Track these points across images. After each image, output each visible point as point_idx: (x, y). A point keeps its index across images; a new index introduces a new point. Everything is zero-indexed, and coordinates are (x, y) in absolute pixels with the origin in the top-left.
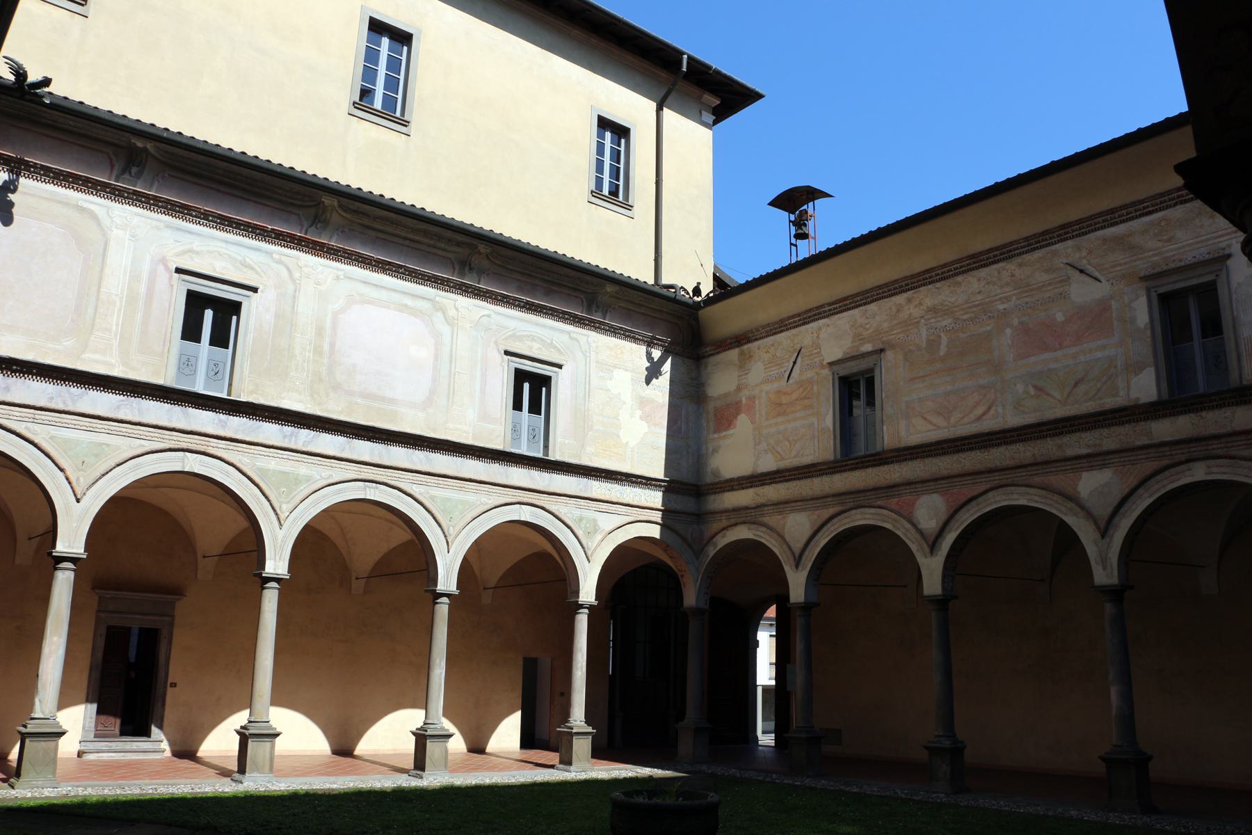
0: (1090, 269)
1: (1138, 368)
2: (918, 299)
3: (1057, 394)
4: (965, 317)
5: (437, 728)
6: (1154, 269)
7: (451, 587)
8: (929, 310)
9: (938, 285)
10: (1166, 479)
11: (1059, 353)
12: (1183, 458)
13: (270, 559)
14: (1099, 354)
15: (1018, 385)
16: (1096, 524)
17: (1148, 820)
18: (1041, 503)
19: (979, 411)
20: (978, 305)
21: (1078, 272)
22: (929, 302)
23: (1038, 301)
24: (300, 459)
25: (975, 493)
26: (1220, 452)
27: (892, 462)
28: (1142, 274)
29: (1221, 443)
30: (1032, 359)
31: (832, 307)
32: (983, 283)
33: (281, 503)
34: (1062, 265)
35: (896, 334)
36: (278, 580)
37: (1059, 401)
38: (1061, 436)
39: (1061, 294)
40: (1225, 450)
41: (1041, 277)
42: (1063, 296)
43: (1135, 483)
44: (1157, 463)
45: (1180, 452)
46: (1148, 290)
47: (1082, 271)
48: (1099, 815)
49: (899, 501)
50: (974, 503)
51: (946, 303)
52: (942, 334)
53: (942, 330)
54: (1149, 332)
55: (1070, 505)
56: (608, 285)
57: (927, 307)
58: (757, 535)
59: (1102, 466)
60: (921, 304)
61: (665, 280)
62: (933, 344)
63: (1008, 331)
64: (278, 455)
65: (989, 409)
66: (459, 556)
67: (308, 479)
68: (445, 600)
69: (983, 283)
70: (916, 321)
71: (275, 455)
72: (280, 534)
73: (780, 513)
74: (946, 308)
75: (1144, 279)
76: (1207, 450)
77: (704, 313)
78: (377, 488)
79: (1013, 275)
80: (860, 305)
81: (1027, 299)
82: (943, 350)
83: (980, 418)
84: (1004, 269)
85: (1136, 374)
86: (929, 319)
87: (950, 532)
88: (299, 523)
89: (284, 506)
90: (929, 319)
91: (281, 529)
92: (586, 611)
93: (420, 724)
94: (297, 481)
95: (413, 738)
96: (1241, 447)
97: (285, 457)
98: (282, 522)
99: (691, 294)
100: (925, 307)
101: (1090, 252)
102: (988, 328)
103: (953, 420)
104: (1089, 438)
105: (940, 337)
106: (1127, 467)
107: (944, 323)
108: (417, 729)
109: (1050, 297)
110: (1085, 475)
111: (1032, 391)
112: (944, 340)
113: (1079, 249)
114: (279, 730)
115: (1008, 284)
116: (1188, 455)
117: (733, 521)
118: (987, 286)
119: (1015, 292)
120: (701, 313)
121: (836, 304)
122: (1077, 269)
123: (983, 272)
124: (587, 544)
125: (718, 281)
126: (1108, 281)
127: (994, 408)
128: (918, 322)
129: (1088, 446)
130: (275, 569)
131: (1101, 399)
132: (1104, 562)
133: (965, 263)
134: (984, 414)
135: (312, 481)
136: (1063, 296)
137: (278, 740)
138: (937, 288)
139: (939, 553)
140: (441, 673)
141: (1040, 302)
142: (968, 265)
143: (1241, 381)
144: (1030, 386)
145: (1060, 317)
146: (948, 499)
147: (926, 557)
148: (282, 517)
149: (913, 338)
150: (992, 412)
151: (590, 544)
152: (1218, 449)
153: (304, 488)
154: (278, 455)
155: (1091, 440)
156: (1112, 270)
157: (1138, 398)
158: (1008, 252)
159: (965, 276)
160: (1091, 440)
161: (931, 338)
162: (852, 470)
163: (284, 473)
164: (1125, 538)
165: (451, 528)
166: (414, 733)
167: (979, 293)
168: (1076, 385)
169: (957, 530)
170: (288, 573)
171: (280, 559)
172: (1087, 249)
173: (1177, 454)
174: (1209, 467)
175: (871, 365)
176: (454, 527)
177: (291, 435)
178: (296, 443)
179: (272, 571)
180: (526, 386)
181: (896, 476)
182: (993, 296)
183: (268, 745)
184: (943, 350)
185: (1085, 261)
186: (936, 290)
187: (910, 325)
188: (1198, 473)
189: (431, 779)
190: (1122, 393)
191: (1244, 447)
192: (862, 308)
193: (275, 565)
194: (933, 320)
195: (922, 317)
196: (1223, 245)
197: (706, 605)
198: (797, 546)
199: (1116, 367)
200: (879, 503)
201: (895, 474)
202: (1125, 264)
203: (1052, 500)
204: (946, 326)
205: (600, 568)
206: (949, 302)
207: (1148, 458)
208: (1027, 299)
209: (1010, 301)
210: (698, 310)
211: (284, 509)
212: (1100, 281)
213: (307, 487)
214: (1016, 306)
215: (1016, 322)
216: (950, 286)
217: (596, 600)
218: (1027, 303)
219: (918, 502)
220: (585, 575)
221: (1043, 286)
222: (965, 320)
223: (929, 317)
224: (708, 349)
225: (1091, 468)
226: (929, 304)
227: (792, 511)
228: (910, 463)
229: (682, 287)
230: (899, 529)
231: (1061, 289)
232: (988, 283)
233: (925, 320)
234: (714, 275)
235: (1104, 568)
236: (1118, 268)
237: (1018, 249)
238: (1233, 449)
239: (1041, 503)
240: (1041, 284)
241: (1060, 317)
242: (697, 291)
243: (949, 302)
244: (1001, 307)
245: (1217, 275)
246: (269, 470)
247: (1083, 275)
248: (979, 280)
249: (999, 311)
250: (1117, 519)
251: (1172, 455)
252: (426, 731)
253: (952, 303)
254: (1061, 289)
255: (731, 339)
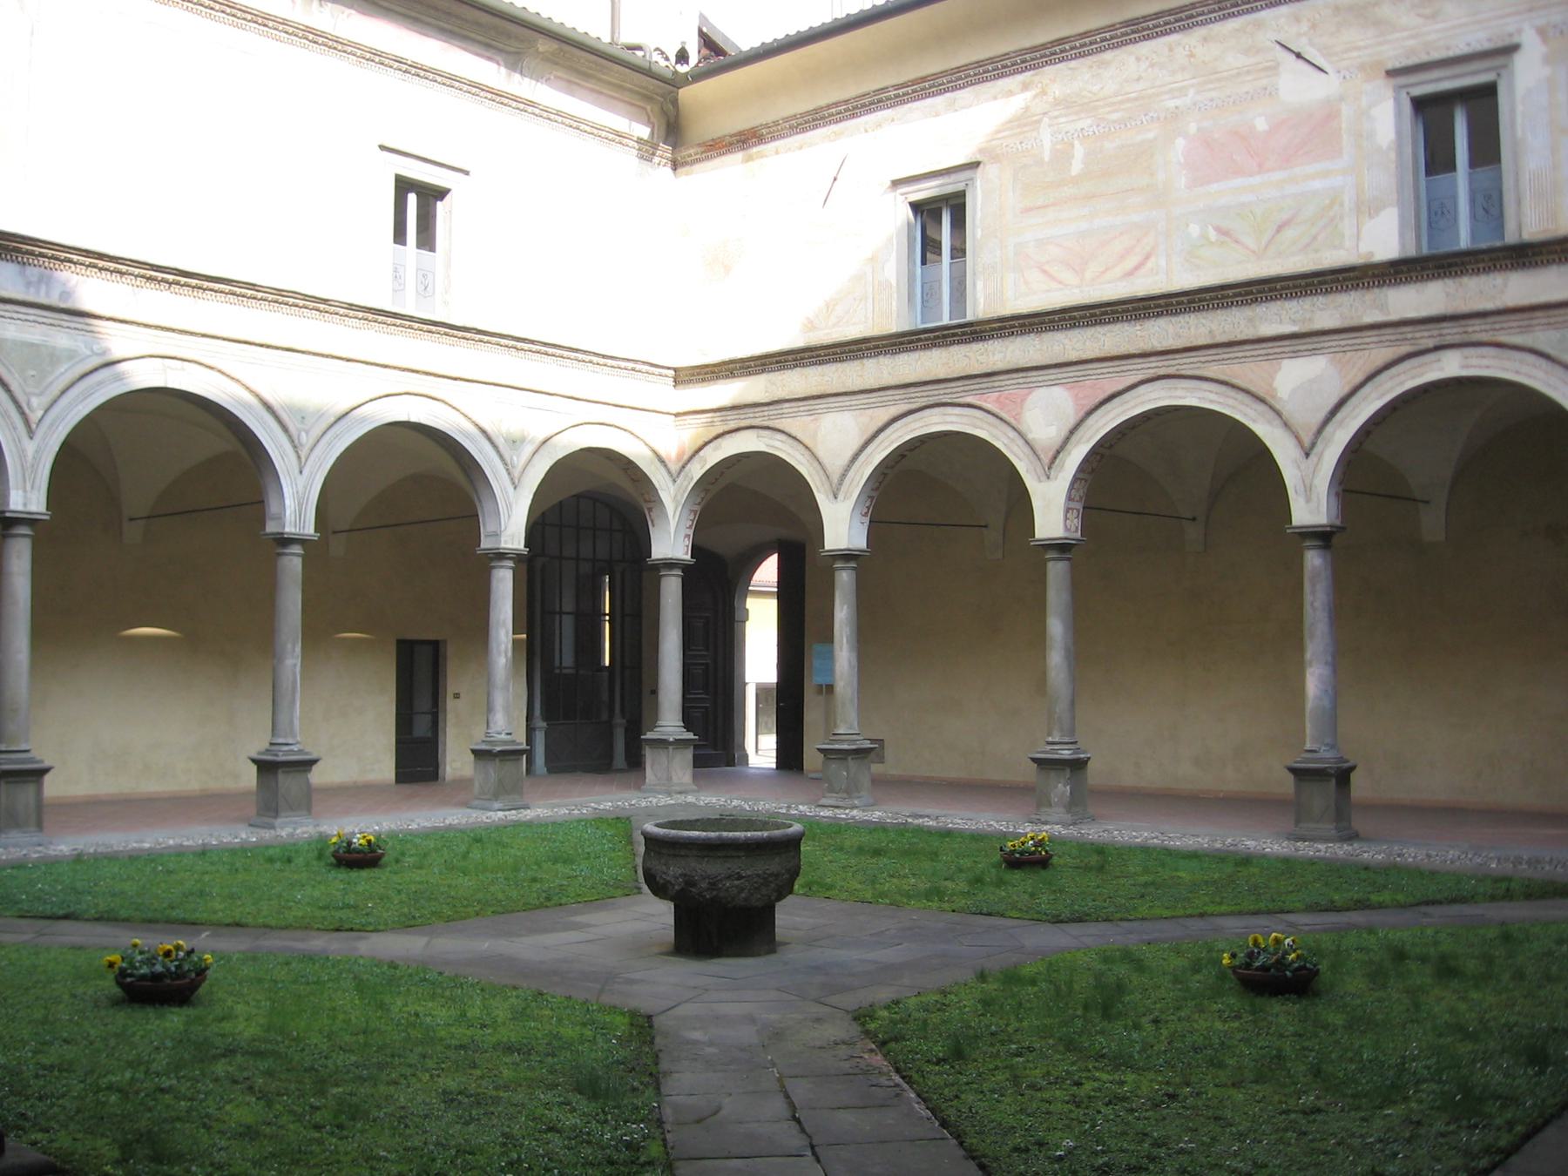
0: (1310, 53)
1: (1367, 208)
2: (1040, 85)
3: (1249, 241)
4: (1115, 116)
5: (292, 751)
6: (1408, 58)
7: (307, 529)
8: (1057, 103)
9: (1073, 64)
10: (1404, 372)
11: (1257, 179)
12: (1430, 343)
13: (17, 489)
14: (1317, 185)
15: (1191, 226)
16: (1297, 438)
17: (1350, 848)
18: (1219, 403)
19: (1130, 263)
20: (1136, 99)
21: (1294, 57)
22: (1056, 90)
23: (1229, 97)
24: (56, 322)
25: (1120, 387)
26: (1484, 337)
27: (992, 337)
28: (1390, 66)
29: (1486, 324)
30: (1214, 187)
31: (900, 92)
32: (1144, 65)
33: (28, 395)
34: (1268, 43)
35: (1003, 138)
36: (30, 521)
37: (1254, 252)
38: (1254, 305)
39: (1266, 89)
40: (1491, 333)
41: (1235, 60)
42: (1268, 92)
43: (1360, 378)
44: (1391, 349)
45: (1426, 334)
46: (1398, 89)
47: (1299, 56)
48: (1284, 845)
49: (1000, 396)
50: (1116, 400)
51: (1084, 93)
52: (1076, 142)
53: (1076, 135)
54: (1393, 155)
55: (1261, 407)
56: (540, 41)
57: (1055, 98)
58: (773, 447)
59: (1314, 352)
60: (1044, 93)
61: (626, 38)
62: (1062, 156)
63: (1180, 143)
64: (21, 316)
65: (1147, 257)
66: (318, 477)
67: (72, 355)
68: (297, 549)
69: (1144, 65)
70: (1035, 118)
71: (15, 316)
72: (30, 447)
73: (811, 413)
74: (1086, 101)
75: (1392, 73)
76: (1466, 332)
77: (686, 94)
78: (183, 369)
79: (1192, 55)
80: (946, 91)
81: (1213, 94)
82: (1076, 167)
83: (1130, 274)
84: (1179, 44)
85: (1371, 216)
86: (1056, 117)
87: (1078, 442)
88: (60, 428)
89: (35, 401)
90: (1056, 117)
91: (31, 438)
92: (510, 564)
93: (265, 745)
94: (54, 357)
95: (254, 768)
96: (1513, 331)
97: (31, 318)
98: (34, 426)
99: (673, 59)
100: (1051, 99)
101: (1314, 27)
102: (1151, 135)
103: (1088, 275)
104: (1294, 310)
105: (1072, 145)
106: (1349, 354)
107: (1079, 125)
108: (259, 753)
109: (1247, 93)
110: (1286, 364)
111: (1213, 235)
112: (1079, 151)
113: (1298, 20)
114: (47, 764)
115: (1183, 69)
116: (1438, 339)
117: (732, 425)
118: (1150, 70)
119: (1194, 81)
120: (686, 94)
121: (908, 86)
122: (1294, 52)
123: (1145, 48)
124: (512, 459)
125: (709, 43)
126: (1339, 72)
127: (1153, 259)
128: (1039, 122)
129: (1294, 321)
130: (25, 505)
131: (1316, 251)
132: (1308, 490)
133: (1118, 32)
134: (1137, 268)
135: (77, 360)
136: (1268, 92)
137: (47, 778)
138: (1070, 69)
139: (1061, 475)
140: (295, 665)
141: (1232, 100)
142: (1123, 35)
143: (1520, 235)
144: (1210, 227)
145: (1261, 125)
146: (1077, 395)
147: (1040, 481)
148: (34, 417)
149: (1029, 147)
150: (1150, 264)
151: (515, 458)
152: (1481, 331)
153: (66, 371)
154: (21, 316)
155: (1298, 312)
156: (1345, 56)
157: (1371, 254)
158: (1188, 18)
159: (1117, 52)
160: (1298, 312)
161: (1059, 147)
162: (926, 347)
163: (32, 345)
164: (1341, 456)
165: (303, 434)
166: (254, 761)
167: (1138, 80)
168: (1279, 229)
169: (1088, 441)
170: (47, 509)
171: (32, 488)
172: (1309, 20)
173: (1422, 338)
174: (1466, 358)
175: (960, 187)
176: (307, 432)
177: (40, 281)
178: (48, 294)
179: (20, 508)
180: (412, 199)
181: (996, 358)
182: (1160, 86)
183: (31, 789)
184: (1076, 167)
185: (1304, 40)
186: (1070, 72)
187: (1025, 125)
188: (1450, 366)
189: (289, 830)
190: (1348, 244)
191: (1518, 330)
192: (948, 95)
193: (25, 497)
194: (1063, 120)
195: (1045, 113)
196: (1511, 29)
197: (687, 553)
198: (836, 464)
199: (1342, 205)
200: (969, 400)
201: (994, 354)
202: (1366, 47)
203: (1236, 399)
204: (1082, 129)
205: (531, 497)
206: (1090, 92)
207: (1381, 342)
208: (1213, 94)
209: (1186, 95)
210: (679, 88)
211: (36, 406)
212: (1326, 73)
213: (70, 368)
214: (1195, 104)
215: (1193, 128)
216: (1091, 67)
217: (525, 547)
218: (1212, 100)
219: (1030, 397)
220: (509, 507)
221: (1238, 74)
222: (1115, 122)
223: (1056, 113)
224: (692, 151)
225: (1295, 354)
226: (1057, 93)
227: (829, 410)
228: (1019, 339)
229: (657, 49)
230: (998, 439)
231: (1264, 82)
232: (1152, 65)
233: (1050, 118)
234: (700, 31)
235: (1308, 500)
236: (1355, 54)
237: (1203, 14)
238: (1502, 332)
239: (1219, 403)
240: (1236, 71)
241: (1261, 125)
242: (682, 56)
243: (1090, 92)
244: (1171, 104)
245: (1499, 75)
246: (6, 340)
247: (1301, 63)
248: (1138, 59)
249: (1168, 109)
250: (1329, 429)
251: (1416, 339)
252: (277, 755)
253: (1095, 94)
254: (1264, 82)
255: (731, 136)
